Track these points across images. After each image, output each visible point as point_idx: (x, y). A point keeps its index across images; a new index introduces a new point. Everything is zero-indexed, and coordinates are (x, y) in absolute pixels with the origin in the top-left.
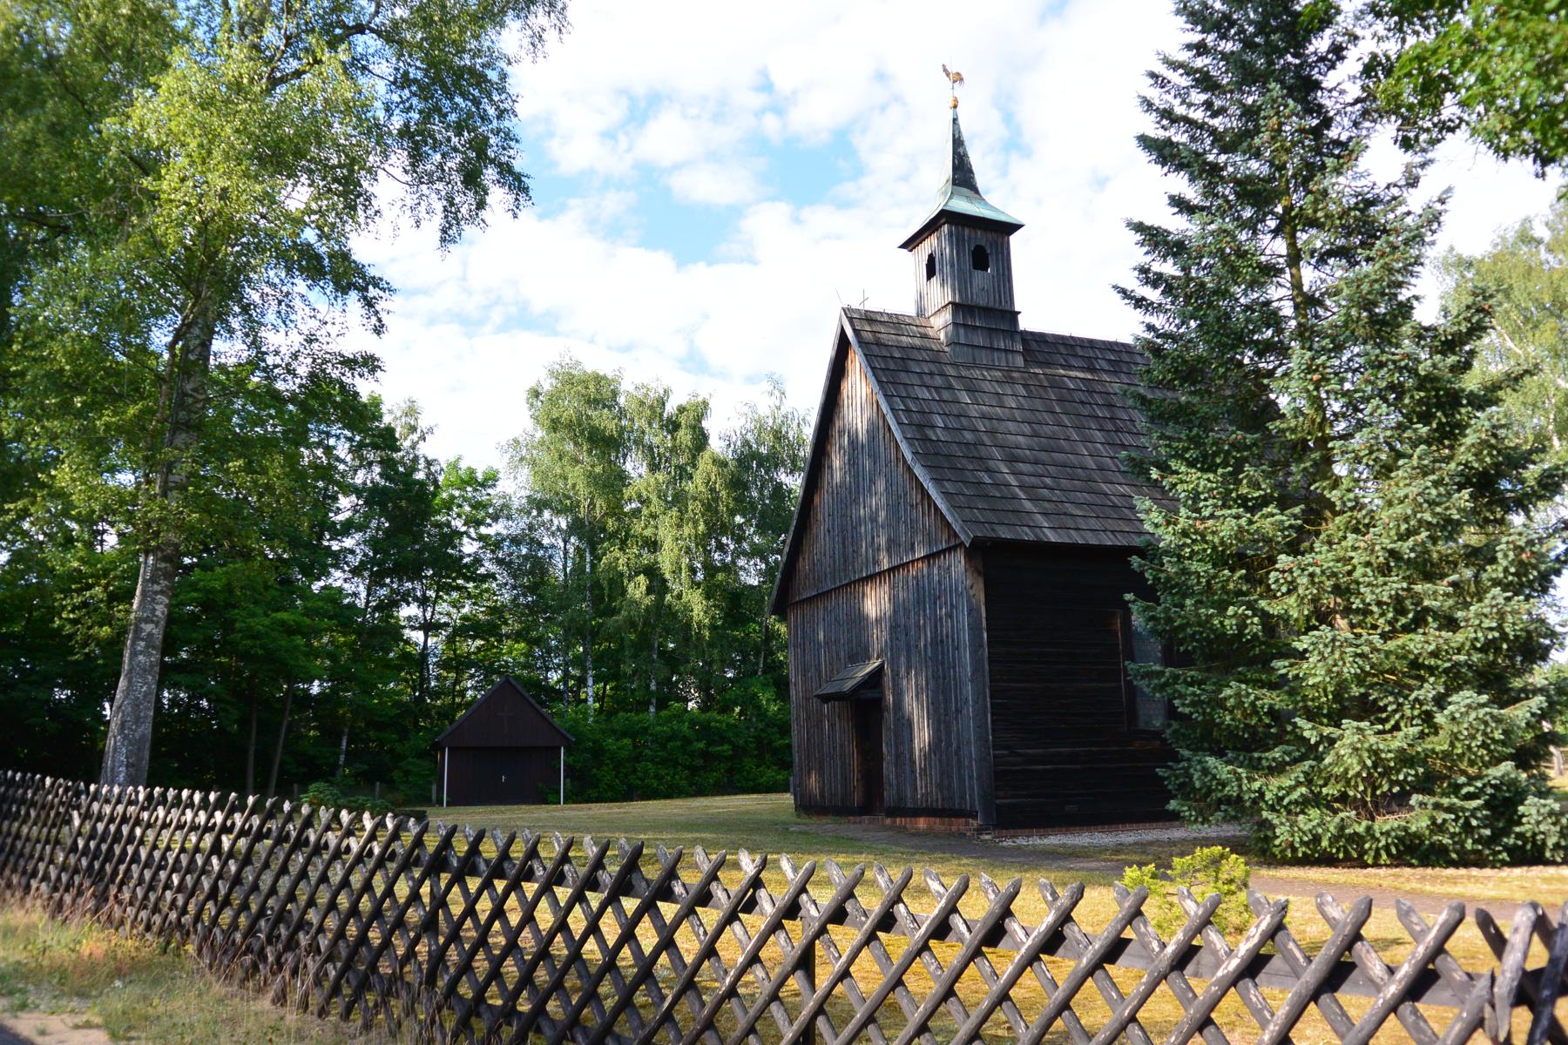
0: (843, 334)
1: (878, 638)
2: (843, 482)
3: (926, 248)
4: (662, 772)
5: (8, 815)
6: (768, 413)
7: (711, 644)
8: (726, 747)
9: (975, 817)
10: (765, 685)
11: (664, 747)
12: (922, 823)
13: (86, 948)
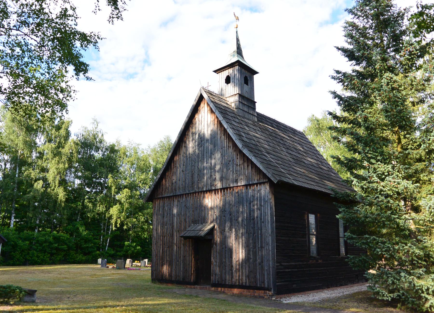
1: (212, 215)
2: (194, 152)
4: (40, 255)
6: (92, 129)
7: (64, 209)
8: (65, 246)
9: (270, 290)
10: (81, 225)
11: (41, 245)
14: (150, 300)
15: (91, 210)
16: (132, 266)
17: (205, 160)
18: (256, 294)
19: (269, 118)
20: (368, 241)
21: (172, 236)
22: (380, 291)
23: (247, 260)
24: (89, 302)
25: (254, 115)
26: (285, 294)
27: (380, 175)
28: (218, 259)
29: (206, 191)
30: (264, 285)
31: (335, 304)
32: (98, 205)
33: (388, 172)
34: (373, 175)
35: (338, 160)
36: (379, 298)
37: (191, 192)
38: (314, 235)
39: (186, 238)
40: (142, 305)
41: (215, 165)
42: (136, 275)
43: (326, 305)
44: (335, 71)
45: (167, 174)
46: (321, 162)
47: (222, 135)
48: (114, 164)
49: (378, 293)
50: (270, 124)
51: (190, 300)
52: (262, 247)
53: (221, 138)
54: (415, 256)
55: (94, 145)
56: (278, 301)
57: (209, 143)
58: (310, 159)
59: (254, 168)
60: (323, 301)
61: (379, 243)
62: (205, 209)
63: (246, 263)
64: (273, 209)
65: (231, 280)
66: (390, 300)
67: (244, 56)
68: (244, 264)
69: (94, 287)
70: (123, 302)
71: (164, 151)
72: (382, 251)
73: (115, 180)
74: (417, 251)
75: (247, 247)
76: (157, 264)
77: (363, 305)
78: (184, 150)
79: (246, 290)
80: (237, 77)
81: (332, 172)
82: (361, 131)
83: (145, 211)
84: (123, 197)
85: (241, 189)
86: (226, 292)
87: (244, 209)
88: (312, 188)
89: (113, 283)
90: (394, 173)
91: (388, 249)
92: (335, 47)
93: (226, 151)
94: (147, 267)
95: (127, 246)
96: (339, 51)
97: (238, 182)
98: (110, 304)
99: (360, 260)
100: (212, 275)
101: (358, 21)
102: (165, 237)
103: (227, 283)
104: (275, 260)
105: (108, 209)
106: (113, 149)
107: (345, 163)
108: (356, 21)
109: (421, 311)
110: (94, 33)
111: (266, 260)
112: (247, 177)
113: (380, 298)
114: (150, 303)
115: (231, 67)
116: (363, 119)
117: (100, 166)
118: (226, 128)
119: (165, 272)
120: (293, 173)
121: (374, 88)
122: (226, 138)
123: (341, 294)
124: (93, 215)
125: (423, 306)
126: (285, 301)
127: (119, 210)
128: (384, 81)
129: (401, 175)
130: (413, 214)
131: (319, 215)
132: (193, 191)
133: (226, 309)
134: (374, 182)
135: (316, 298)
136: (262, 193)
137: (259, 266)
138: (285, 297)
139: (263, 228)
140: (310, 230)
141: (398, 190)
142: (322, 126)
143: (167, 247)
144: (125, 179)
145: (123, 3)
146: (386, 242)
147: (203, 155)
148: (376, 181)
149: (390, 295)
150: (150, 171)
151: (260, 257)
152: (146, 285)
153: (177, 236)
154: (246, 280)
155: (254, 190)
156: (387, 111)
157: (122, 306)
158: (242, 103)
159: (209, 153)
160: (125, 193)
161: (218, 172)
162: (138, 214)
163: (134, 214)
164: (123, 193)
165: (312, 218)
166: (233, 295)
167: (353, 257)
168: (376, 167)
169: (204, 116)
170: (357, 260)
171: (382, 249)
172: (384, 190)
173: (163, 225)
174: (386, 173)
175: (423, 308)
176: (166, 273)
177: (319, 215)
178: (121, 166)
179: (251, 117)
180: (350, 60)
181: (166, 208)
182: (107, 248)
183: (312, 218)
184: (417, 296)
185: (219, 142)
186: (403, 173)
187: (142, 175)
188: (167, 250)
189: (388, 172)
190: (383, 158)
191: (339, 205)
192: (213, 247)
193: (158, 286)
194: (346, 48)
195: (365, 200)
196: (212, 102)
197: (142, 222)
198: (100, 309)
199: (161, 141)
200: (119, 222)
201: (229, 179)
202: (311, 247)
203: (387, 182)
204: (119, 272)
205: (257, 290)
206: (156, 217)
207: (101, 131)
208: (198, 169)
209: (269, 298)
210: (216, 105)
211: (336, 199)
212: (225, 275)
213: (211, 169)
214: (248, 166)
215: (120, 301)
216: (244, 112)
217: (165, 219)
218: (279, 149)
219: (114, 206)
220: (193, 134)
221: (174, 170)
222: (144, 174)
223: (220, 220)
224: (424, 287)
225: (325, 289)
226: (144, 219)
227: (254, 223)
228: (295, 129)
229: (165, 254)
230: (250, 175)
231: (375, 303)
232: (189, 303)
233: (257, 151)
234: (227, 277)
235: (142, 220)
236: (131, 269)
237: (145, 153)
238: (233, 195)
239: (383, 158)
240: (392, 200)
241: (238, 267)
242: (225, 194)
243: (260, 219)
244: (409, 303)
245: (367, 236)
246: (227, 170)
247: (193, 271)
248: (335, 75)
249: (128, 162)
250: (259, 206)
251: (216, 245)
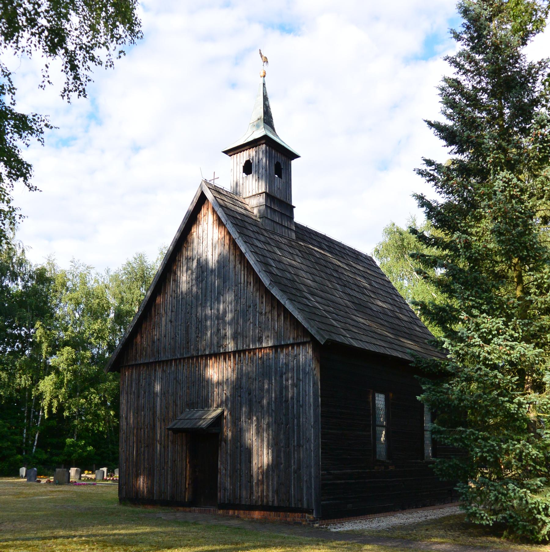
2: (190, 290)
3: (244, 157)
9: (311, 513)
12: (257, 515)
14: (123, 529)
15: (5, 384)
16: (80, 479)
17: (208, 304)
18: (288, 519)
19: (316, 232)
20: (463, 436)
21: (154, 427)
22: (478, 511)
23: (274, 466)
24: (28, 531)
25: (291, 229)
26: (334, 518)
27: (485, 335)
28: (229, 465)
29: (210, 356)
30: (302, 504)
31: (410, 532)
32: (18, 376)
33: (498, 329)
34: (474, 335)
35: (423, 306)
36: (476, 522)
37: (185, 356)
38: (383, 426)
39: (176, 431)
40: (111, 535)
41: (225, 312)
42: (90, 493)
43: (397, 533)
44: (424, 160)
45: (144, 326)
46: (400, 308)
47: (238, 262)
48: (46, 303)
49: (474, 514)
51: (185, 529)
52: (299, 445)
53: (235, 267)
54: (531, 459)
55: (8, 270)
56: (323, 528)
57: (215, 276)
58: (380, 303)
59: (289, 319)
60: (394, 528)
61: (479, 439)
62: (208, 384)
63: (273, 471)
64: (318, 385)
65: (250, 496)
66: (491, 525)
67: (275, 127)
68: (271, 472)
69: (26, 512)
70: (80, 530)
71: (134, 281)
72: (483, 452)
73: (48, 332)
74: (534, 452)
75: (275, 445)
76: (129, 474)
77: (453, 533)
78: (174, 286)
79: (273, 514)
80: (264, 164)
81: (417, 325)
82: (462, 264)
83: (102, 386)
84: (62, 362)
85: (266, 353)
86: (242, 516)
87: (272, 385)
88: (382, 352)
89: (56, 506)
90: (507, 331)
91: (492, 448)
92: (426, 121)
93: (244, 290)
94: (106, 480)
95: (71, 446)
96: (431, 128)
97: (262, 342)
98: (61, 533)
99: (450, 466)
100: (219, 490)
101: (466, 78)
102: (141, 430)
103: (243, 503)
104: (319, 465)
105: (35, 383)
106: (43, 277)
107: (433, 314)
108: (462, 78)
109: (536, 540)
110: (38, 116)
111: (305, 466)
112: (277, 333)
113: (477, 522)
114: (123, 532)
115: (252, 145)
116: (463, 245)
117: (20, 307)
118: (244, 251)
119: (141, 486)
120: (351, 328)
121: (484, 194)
122: (244, 269)
123: (423, 519)
124: (10, 393)
125: (539, 533)
126: (335, 528)
127: (55, 384)
128: (498, 184)
129: (517, 335)
130: (533, 396)
131: (391, 395)
132: (188, 356)
133: (242, 540)
134: (475, 346)
135: (382, 524)
136: (301, 360)
137: (294, 475)
138: (335, 524)
139: (301, 415)
140: (377, 419)
141: (511, 358)
142: (408, 244)
143: (145, 447)
144: (66, 330)
145: (86, 69)
146: (489, 438)
147: (205, 296)
148: (478, 343)
149: (492, 517)
150: (108, 315)
151: (296, 460)
152: (111, 509)
153: (161, 428)
154: (273, 497)
155: (287, 355)
156: (500, 234)
157: (81, 536)
158: (271, 208)
159: (215, 291)
160: (65, 355)
161: (230, 324)
162: (89, 391)
163: (82, 391)
164: (62, 355)
165: (380, 400)
166: (253, 521)
167: (440, 462)
168: (479, 321)
169: (206, 229)
170: (446, 465)
171: (483, 449)
172: (490, 358)
173: (137, 411)
174: (494, 331)
175: (539, 536)
176: (143, 488)
177: (391, 395)
178: (57, 306)
179: (285, 232)
180: (450, 143)
181: (143, 383)
182: (34, 450)
183: (380, 400)
184: (530, 518)
185: (232, 274)
186: (520, 331)
187: (94, 323)
188: (144, 451)
189: (498, 329)
190: (492, 307)
191: (423, 379)
192: (221, 446)
193: (131, 509)
194: (443, 124)
195: (460, 374)
196: (221, 206)
197: (96, 405)
198: (47, 541)
199: (129, 264)
200: (55, 404)
201: (248, 336)
202: (378, 446)
203: (494, 345)
204: (61, 489)
205: (290, 512)
206: (125, 398)
207: (21, 245)
208: (197, 318)
209: (309, 524)
210: (228, 212)
211: (418, 370)
212: (240, 489)
213: (218, 318)
214: (279, 316)
215: (76, 531)
216: (275, 225)
217: (142, 401)
218: (330, 286)
219: (46, 377)
220: (190, 259)
221: (156, 319)
222: (99, 321)
223: (233, 403)
224: (541, 505)
225: (398, 511)
226: (100, 399)
227: (287, 408)
228: (358, 252)
229: (142, 457)
230: (282, 330)
231: (472, 531)
232: (184, 531)
233: (294, 291)
234: (244, 493)
235: (96, 400)
236: (79, 485)
237: (100, 283)
238: (254, 362)
239: (491, 307)
240: (500, 374)
241: (260, 477)
242: (241, 361)
243: (297, 401)
244: (518, 529)
245: (461, 429)
246: (245, 321)
247: (188, 484)
248: (425, 167)
249: (71, 300)
250: (295, 381)
251: (226, 443)
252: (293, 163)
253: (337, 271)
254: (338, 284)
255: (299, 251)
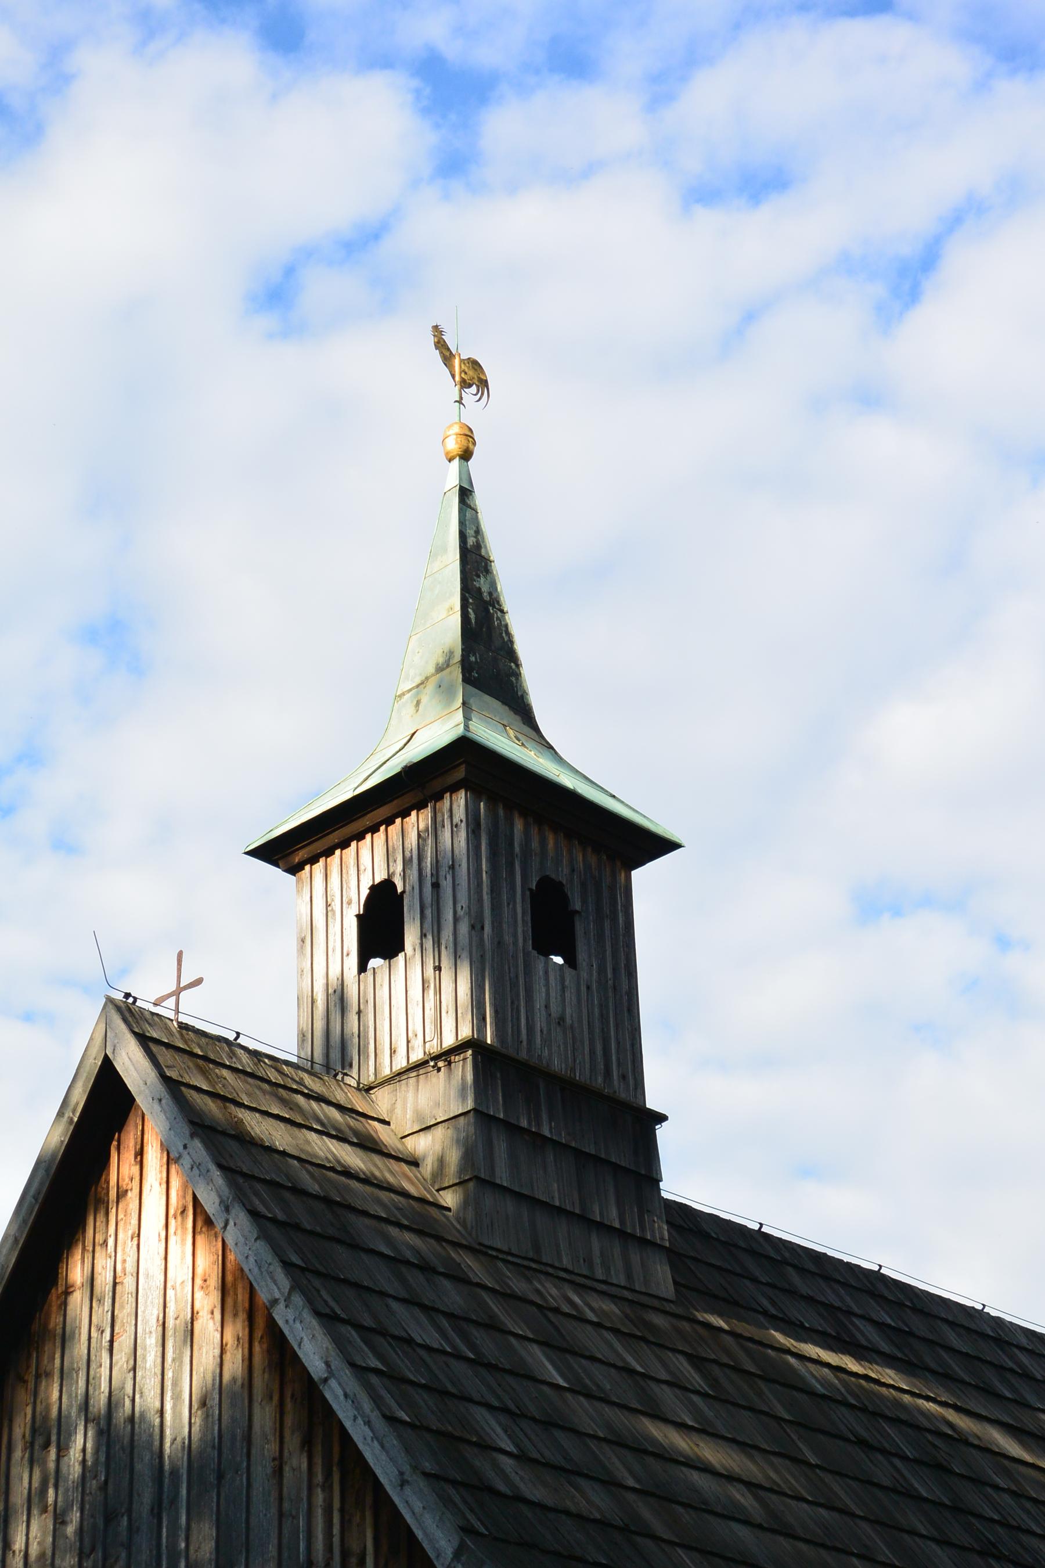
0: (108, 1071)
5: (310, 1563)
13: (49, 1499)
25: (644, 1243)
47: (293, 1441)
50: (819, 1324)
53: (279, 1472)
122: (328, 1475)
158: (512, 1129)
169: (130, 1267)
252: (640, 877)
253: (940, 1468)
254: (944, 1542)
255: (696, 1360)
